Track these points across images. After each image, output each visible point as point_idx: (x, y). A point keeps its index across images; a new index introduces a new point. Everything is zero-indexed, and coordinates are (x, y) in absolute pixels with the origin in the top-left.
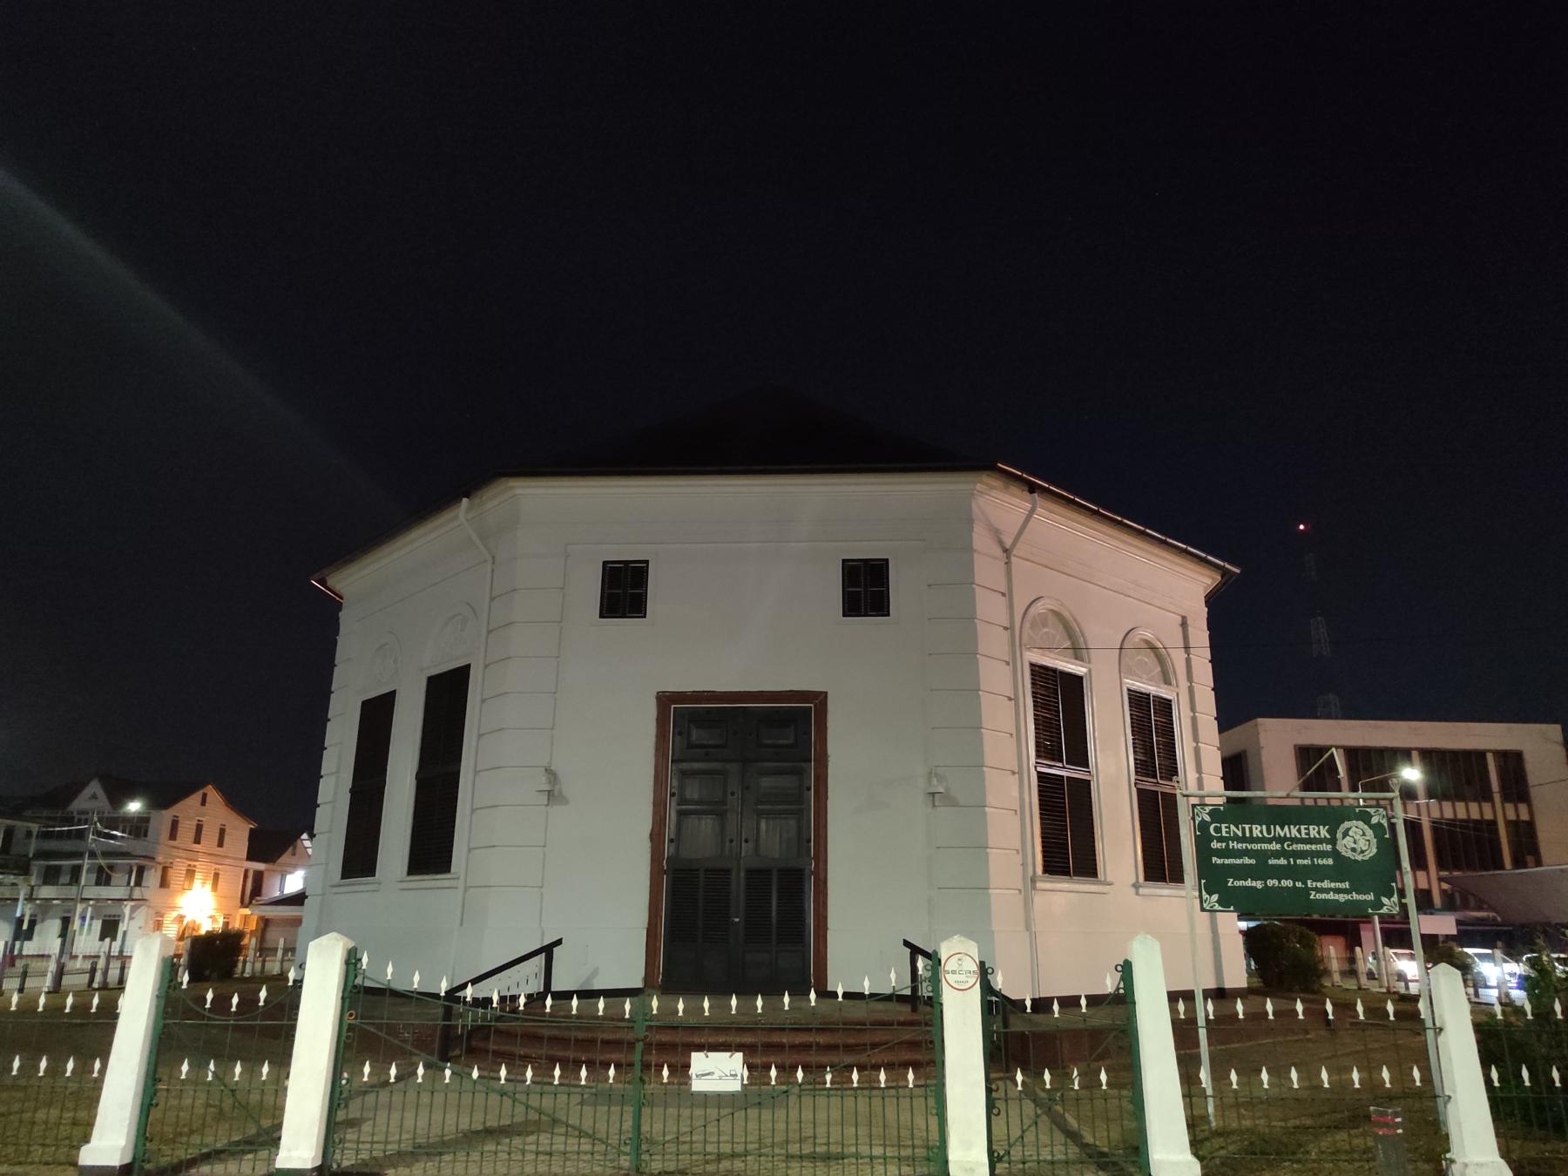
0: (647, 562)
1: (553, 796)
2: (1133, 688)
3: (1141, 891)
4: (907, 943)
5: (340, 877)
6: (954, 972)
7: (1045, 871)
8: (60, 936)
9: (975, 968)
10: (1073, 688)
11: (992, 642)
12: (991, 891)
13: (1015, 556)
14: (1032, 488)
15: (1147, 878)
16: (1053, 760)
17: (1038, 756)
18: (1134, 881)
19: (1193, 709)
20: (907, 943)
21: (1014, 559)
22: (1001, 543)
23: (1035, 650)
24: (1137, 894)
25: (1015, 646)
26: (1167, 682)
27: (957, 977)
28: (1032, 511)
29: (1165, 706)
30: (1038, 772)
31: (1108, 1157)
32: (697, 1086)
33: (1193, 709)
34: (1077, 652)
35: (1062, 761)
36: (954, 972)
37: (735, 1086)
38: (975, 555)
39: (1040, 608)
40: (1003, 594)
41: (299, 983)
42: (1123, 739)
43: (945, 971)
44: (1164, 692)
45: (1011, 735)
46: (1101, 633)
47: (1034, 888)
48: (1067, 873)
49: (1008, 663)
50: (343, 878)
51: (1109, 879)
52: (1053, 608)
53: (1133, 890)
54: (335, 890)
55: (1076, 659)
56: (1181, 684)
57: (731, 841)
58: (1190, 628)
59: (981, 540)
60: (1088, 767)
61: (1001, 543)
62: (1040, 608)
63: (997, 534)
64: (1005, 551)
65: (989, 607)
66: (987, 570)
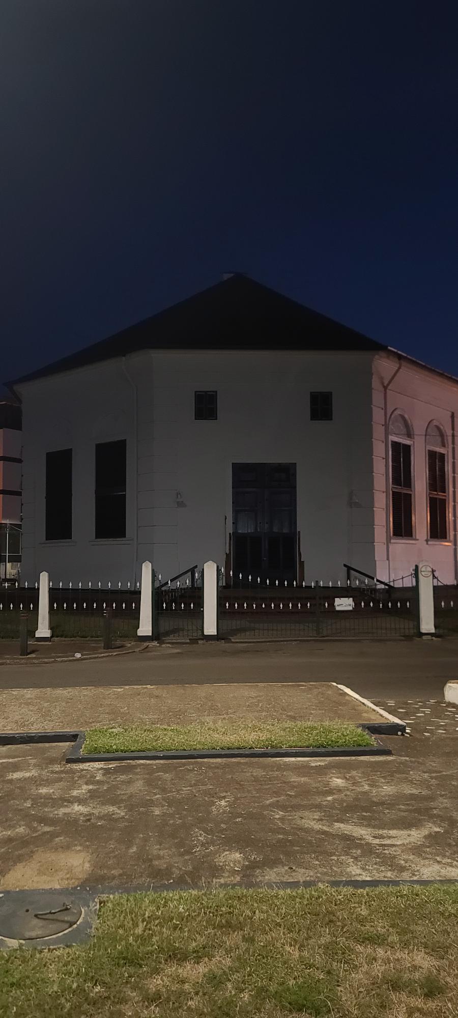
0: (216, 392)
1: (181, 504)
2: (431, 449)
3: (429, 543)
4: (345, 565)
5: (45, 539)
6: (424, 571)
7: (394, 535)
8: (303, 562)
9: (431, 570)
10: (407, 448)
11: (378, 431)
12: (375, 544)
13: (389, 390)
14: (400, 357)
15: (431, 537)
16: (397, 485)
17: (393, 484)
18: (426, 538)
19: (454, 458)
20: (345, 565)
21: (388, 391)
22: (383, 383)
23: (393, 435)
24: (427, 544)
25: (387, 434)
26: (444, 445)
27: (426, 573)
28: (399, 368)
29: (442, 457)
30: (393, 491)
31: (24, 811)
32: (338, 608)
33: (454, 458)
34: (409, 435)
35: (401, 486)
36: (424, 571)
37: (351, 608)
38: (373, 391)
39: (397, 412)
40: (382, 409)
41: (38, 589)
42: (425, 474)
43: (421, 571)
44: (442, 450)
45: (383, 475)
46: (419, 427)
47: (390, 543)
48: (402, 536)
49: (383, 442)
50: (46, 540)
51: (417, 538)
52: (401, 414)
53: (425, 543)
54: (43, 545)
55: (408, 437)
56: (449, 447)
57: (260, 523)
58: (455, 418)
59: (375, 383)
60: (411, 488)
61: (383, 383)
62: (396, 413)
63: (381, 379)
64: (384, 387)
65: (378, 415)
66: (377, 398)
